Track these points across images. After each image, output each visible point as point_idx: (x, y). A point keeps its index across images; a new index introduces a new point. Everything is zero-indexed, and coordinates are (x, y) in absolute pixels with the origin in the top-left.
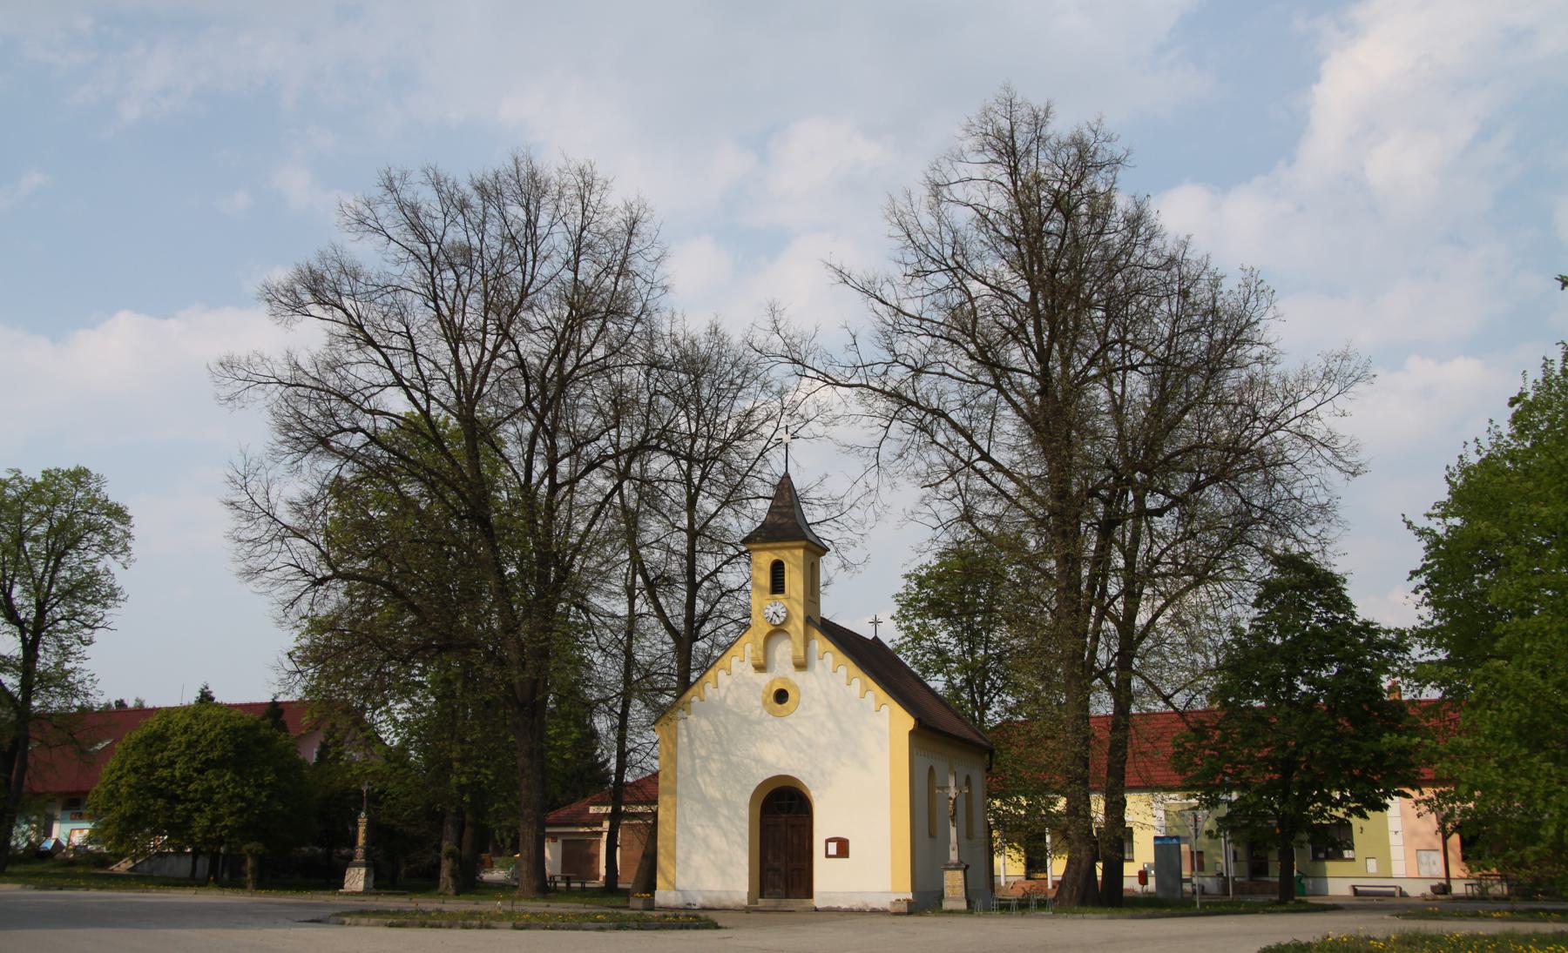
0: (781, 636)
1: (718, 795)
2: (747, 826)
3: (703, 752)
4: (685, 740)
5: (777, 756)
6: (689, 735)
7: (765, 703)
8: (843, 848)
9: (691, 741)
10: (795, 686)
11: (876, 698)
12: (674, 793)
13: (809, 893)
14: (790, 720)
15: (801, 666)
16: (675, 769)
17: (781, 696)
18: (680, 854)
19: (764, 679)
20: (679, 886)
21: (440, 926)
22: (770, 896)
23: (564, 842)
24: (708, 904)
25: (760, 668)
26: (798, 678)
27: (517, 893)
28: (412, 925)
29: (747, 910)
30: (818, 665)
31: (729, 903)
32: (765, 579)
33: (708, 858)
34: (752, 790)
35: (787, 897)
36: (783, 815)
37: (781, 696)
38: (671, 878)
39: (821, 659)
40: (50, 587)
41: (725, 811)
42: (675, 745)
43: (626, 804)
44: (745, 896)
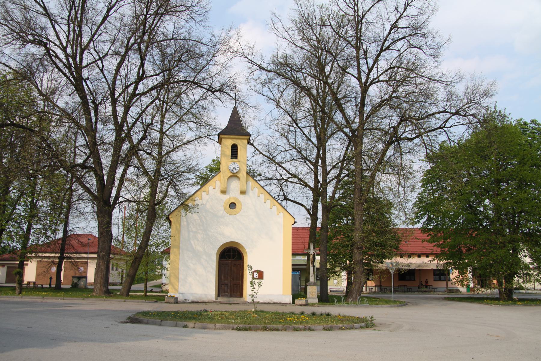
0: (234, 178)
1: (201, 250)
2: (215, 264)
3: (194, 230)
4: (185, 223)
5: (229, 233)
6: (187, 221)
7: (225, 209)
8: (261, 275)
9: (188, 224)
10: (240, 202)
11: (277, 209)
12: (178, 247)
13: (241, 295)
14: (238, 216)
15: (243, 193)
16: (179, 237)
17: (233, 205)
18: (181, 276)
19: (225, 197)
20: (180, 291)
21: (277, 330)
22: (223, 296)
23: (8, 267)
24: (195, 300)
25: (223, 192)
26: (241, 198)
27: (94, 294)
28: (257, 329)
29: (214, 302)
30: (250, 193)
31: (206, 299)
32: (229, 152)
33: (193, 278)
34: (218, 247)
35: (231, 296)
36: (231, 259)
37: (233, 205)
38: (176, 287)
39: (252, 190)
40: (358, 19)
41: (204, 257)
42: (180, 225)
43: (68, 253)
44: (214, 296)
